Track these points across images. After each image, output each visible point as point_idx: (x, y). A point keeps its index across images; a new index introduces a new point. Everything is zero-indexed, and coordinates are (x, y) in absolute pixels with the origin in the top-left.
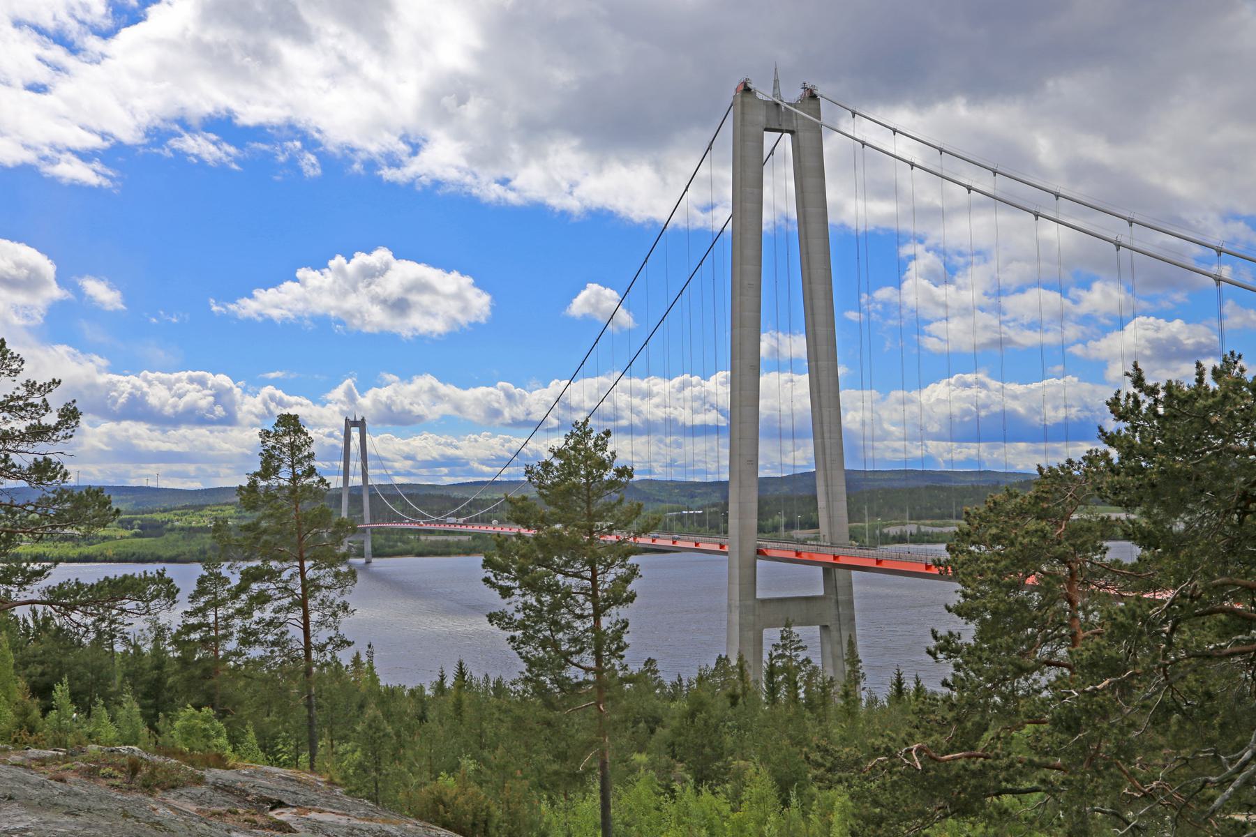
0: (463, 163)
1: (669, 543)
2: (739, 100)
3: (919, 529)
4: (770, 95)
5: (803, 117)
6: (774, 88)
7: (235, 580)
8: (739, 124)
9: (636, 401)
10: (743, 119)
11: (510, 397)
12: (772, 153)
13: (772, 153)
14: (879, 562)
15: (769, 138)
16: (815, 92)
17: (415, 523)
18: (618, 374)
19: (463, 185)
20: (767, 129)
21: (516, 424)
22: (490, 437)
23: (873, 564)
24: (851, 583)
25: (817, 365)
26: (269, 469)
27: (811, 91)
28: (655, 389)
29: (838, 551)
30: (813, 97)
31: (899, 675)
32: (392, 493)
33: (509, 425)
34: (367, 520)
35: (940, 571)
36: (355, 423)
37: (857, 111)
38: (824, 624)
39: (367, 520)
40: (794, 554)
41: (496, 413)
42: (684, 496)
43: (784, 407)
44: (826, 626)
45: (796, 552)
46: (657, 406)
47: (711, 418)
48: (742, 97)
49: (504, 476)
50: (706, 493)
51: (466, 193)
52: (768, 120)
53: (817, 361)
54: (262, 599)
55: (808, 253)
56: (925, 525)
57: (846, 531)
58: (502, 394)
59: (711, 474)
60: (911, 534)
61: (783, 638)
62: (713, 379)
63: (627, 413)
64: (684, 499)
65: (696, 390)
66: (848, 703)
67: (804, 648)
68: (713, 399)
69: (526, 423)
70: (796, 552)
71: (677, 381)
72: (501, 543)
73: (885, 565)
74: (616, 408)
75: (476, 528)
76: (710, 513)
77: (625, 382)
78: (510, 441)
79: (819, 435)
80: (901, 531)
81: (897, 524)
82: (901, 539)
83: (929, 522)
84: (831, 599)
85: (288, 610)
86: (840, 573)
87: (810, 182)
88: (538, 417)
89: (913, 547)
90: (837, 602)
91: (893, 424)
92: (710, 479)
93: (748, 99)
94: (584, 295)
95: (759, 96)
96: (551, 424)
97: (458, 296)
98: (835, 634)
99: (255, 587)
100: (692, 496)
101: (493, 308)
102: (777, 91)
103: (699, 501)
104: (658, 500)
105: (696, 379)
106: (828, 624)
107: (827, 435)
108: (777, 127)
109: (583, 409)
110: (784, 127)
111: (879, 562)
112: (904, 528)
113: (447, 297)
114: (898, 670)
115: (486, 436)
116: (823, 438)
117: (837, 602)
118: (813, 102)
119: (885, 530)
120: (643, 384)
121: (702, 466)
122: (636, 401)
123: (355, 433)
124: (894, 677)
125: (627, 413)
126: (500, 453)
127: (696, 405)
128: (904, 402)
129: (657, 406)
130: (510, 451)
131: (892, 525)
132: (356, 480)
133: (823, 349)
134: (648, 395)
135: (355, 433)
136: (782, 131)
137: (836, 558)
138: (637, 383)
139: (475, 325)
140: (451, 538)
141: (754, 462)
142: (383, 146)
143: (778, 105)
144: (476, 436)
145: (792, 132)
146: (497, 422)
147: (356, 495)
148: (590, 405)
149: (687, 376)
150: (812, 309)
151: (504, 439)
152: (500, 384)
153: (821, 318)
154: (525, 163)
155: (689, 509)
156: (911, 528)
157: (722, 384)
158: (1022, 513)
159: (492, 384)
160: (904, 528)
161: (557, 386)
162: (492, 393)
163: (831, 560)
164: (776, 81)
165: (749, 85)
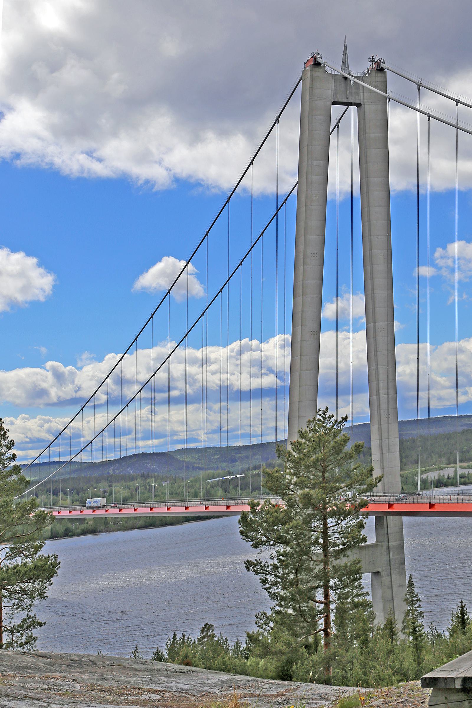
0: (46, 134)
1: (224, 509)
2: (309, 74)
3: (456, 472)
4: (340, 70)
5: (370, 90)
6: (343, 62)
8: (308, 97)
9: (193, 370)
10: (312, 94)
11: (59, 376)
12: (337, 125)
13: (337, 125)
14: (432, 506)
15: (337, 110)
16: (382, 65)
18: (173, 344)
19: (44, 156)
20: (334, 103)
21: (62, 403)
22: (28, 419)
23: (427, 509)
24: (402, 528)
25: (374, 326)
27: (379, 64)
28: (213, 356)
29: (393, 500)
30: (381, 70)
31: (462, 607)
33: (54, 405)
37: (423, 83)
38: (376, 570)
41: (42, 393)
42: (224, 461)
43: (341, 365)
44: (378, 573)
46: (213, 373)
47: (268, 381)
48: (312, 71)
49: (46, 457)
50: (247, 457)
51: (47, 164)
52: (336, 94)
53: (375, 322)
55: (369, 221)
56: (461, 467)
57: (399, 479)
58: (50, 375)
59: (255, 436)
60: (448, 478)
62: (272, 341)
63: (181, 384)
64: (224, 464)
65: (256, 355)
66: (415, 638)
68: (271, 363)
69: (74, 401)
71: (235, 345)
73: (437, 509)
74: (171, 379)
76: (253, 476)
77: (181, 352)
78: (49, 421)
79: (374, 392)
81: (436, 469)
82: (439, 484)
83: (465, 464)
84: (382, 546)
86: (392, 520)
87: (374, 152)
88: (87, 394)
89: (436, 490)
90: (388, 548)
91: (442, 375)
92: (255, 441)
93: (318, 72)
94: (159, 266)
95: (329, 70)
96: (99, 399)
97: (22, 274)
98: (386, 579)
100: (234, 461)
101: (54, 287)
102: (345, 65)
103: (239, 466)
104: (198, 468)
105: (255, 343)
106: (380, 570)
107: (382, 392)
108: (345, 100)
109: (136, 382)
110: (352, 101)
111: (432, 506)
112: (442, 473)
113: (11, 275)
114: (461, 603)
115: (23, 418)
116: (378, 394)
117: (388, 548)
118: (380, 75)
119: (424, 476)
120: (199, 354)
121: (247, 430)
122: (193, 370)
124: (457, 611)
125: (181, 384)
126: (37, 435)
127: (255, 370)
128: (457, 351)
129: (213, 373)
130: (49, 431)
131: (430, 470)
133: (381, 310)
134: (206, 361)
136: (349, 104)
137: (390, 506)
138: (191, 352)
139: (35, 305)
143: (346, 78)
144: (12, 419)
145: (358, 105)
146: (41, 401)
148: (144, 376)
149: (245, 341)
150: (373, 273)
151: (44, 420)
152: (50, 364)
153: (380, 281)
154: (115, 134)
155: (229, 474)
156: (449, 472)
157: (283, 347)
159: (39, 363)
160: (442, 473)
161: (111, 359)
162: (37, 374)
164: (345, 55)
165: (319, 60)
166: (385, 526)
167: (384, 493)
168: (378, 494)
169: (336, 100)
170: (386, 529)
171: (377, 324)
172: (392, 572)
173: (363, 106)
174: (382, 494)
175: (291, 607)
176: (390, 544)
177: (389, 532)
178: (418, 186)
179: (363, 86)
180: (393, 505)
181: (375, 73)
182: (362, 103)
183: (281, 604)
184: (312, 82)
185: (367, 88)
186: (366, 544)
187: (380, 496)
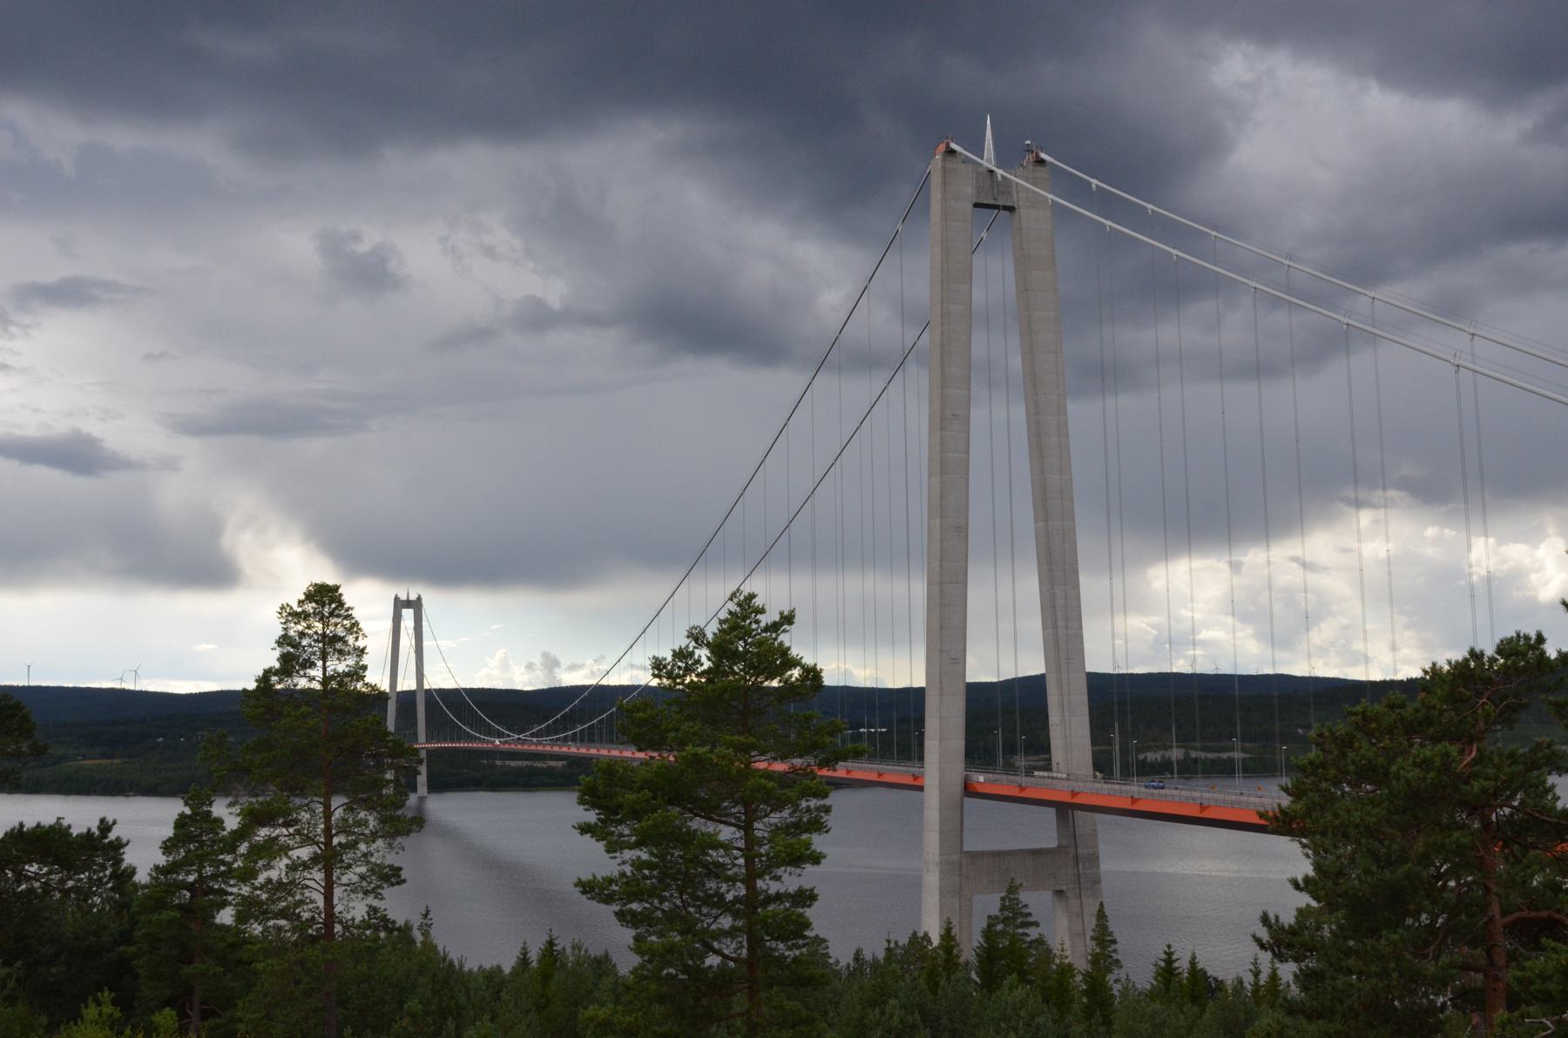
3: (1187, 754)
5: (1026, 188)
7: (232, 823)
17: (488, 742)
26: (291, 662)
32: (453, 698)
34: (422, 736)
35: (1280, 824)
36: (408, 604)
39: (422, 736)
40: (876, 775)
45: (914, 775)
54: (271, 850)
56: (1195, 749)
61: (1003, 908)
67: (1036, 924)
70: (914, 775)
72: (613, 774)
75: (574, 750)
80: (1163, 756)
85: (306, 866)
99: (263, 833)
106: (1064, 888)
108: (992, 202)
114: (1169, 947)
123: (408, 614)
132: (407, 683)
135: (408, 614)
140: (539, 764)
141: (960, 661)
142: (426, 929)
147: (407, 699)
158: (1411, 729)
163: (1067, 799)
166: (1071, 824)
167: (1068, 775)
168: (1060, 775)
169: (980, 201)
170: (1072, 829)
171: (1050, 523)
172: (1082, 892)
173: (1017, 211)
174: (1065, 776)
175: (991, 942)
176: (1079, 851)
177: (1077, 833)
178: (1168, 590)
179: (1017, 183)
180: (1078, 793)
181: (1034, 166)
182: (1016, 206)
183: (561, 966)
184: (945, 188)
185: (1022, 185)
186: (831, 773)
187: (1062, 779)
